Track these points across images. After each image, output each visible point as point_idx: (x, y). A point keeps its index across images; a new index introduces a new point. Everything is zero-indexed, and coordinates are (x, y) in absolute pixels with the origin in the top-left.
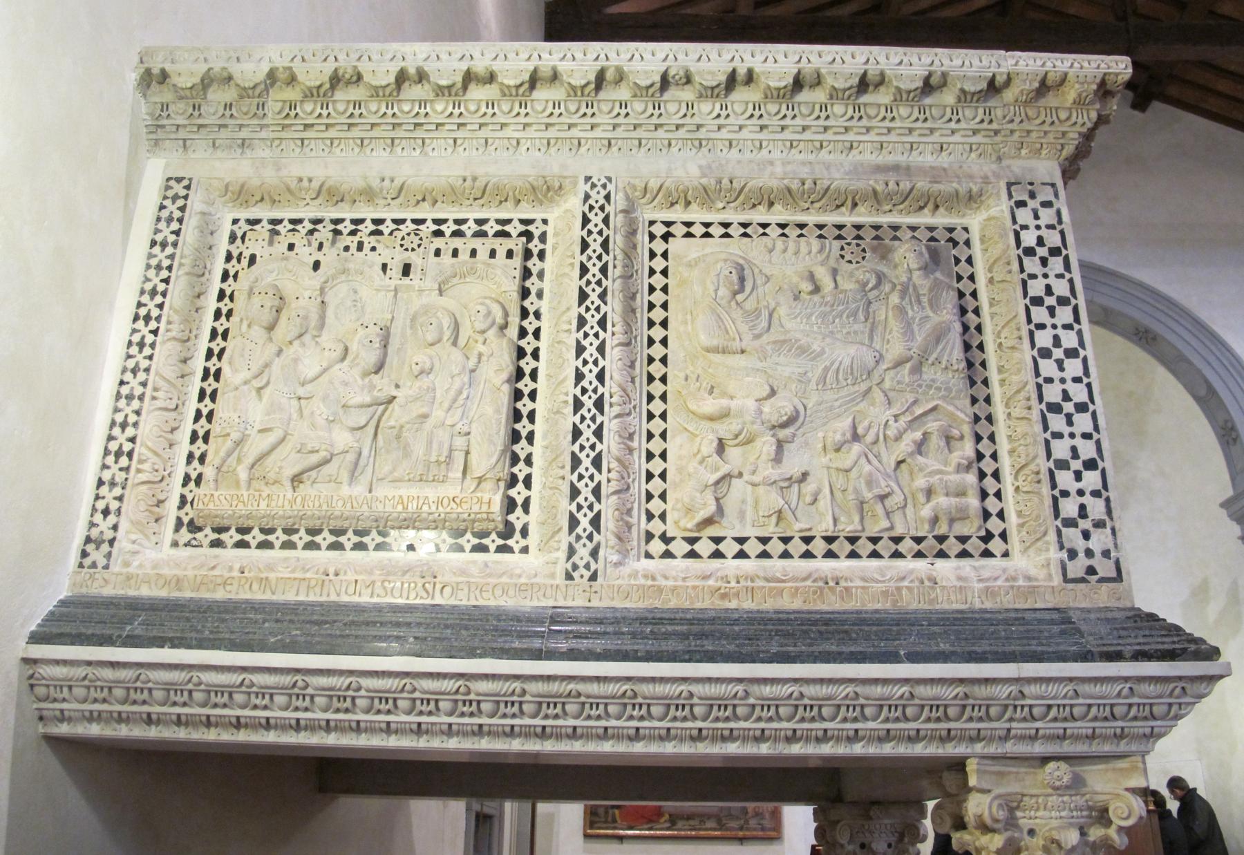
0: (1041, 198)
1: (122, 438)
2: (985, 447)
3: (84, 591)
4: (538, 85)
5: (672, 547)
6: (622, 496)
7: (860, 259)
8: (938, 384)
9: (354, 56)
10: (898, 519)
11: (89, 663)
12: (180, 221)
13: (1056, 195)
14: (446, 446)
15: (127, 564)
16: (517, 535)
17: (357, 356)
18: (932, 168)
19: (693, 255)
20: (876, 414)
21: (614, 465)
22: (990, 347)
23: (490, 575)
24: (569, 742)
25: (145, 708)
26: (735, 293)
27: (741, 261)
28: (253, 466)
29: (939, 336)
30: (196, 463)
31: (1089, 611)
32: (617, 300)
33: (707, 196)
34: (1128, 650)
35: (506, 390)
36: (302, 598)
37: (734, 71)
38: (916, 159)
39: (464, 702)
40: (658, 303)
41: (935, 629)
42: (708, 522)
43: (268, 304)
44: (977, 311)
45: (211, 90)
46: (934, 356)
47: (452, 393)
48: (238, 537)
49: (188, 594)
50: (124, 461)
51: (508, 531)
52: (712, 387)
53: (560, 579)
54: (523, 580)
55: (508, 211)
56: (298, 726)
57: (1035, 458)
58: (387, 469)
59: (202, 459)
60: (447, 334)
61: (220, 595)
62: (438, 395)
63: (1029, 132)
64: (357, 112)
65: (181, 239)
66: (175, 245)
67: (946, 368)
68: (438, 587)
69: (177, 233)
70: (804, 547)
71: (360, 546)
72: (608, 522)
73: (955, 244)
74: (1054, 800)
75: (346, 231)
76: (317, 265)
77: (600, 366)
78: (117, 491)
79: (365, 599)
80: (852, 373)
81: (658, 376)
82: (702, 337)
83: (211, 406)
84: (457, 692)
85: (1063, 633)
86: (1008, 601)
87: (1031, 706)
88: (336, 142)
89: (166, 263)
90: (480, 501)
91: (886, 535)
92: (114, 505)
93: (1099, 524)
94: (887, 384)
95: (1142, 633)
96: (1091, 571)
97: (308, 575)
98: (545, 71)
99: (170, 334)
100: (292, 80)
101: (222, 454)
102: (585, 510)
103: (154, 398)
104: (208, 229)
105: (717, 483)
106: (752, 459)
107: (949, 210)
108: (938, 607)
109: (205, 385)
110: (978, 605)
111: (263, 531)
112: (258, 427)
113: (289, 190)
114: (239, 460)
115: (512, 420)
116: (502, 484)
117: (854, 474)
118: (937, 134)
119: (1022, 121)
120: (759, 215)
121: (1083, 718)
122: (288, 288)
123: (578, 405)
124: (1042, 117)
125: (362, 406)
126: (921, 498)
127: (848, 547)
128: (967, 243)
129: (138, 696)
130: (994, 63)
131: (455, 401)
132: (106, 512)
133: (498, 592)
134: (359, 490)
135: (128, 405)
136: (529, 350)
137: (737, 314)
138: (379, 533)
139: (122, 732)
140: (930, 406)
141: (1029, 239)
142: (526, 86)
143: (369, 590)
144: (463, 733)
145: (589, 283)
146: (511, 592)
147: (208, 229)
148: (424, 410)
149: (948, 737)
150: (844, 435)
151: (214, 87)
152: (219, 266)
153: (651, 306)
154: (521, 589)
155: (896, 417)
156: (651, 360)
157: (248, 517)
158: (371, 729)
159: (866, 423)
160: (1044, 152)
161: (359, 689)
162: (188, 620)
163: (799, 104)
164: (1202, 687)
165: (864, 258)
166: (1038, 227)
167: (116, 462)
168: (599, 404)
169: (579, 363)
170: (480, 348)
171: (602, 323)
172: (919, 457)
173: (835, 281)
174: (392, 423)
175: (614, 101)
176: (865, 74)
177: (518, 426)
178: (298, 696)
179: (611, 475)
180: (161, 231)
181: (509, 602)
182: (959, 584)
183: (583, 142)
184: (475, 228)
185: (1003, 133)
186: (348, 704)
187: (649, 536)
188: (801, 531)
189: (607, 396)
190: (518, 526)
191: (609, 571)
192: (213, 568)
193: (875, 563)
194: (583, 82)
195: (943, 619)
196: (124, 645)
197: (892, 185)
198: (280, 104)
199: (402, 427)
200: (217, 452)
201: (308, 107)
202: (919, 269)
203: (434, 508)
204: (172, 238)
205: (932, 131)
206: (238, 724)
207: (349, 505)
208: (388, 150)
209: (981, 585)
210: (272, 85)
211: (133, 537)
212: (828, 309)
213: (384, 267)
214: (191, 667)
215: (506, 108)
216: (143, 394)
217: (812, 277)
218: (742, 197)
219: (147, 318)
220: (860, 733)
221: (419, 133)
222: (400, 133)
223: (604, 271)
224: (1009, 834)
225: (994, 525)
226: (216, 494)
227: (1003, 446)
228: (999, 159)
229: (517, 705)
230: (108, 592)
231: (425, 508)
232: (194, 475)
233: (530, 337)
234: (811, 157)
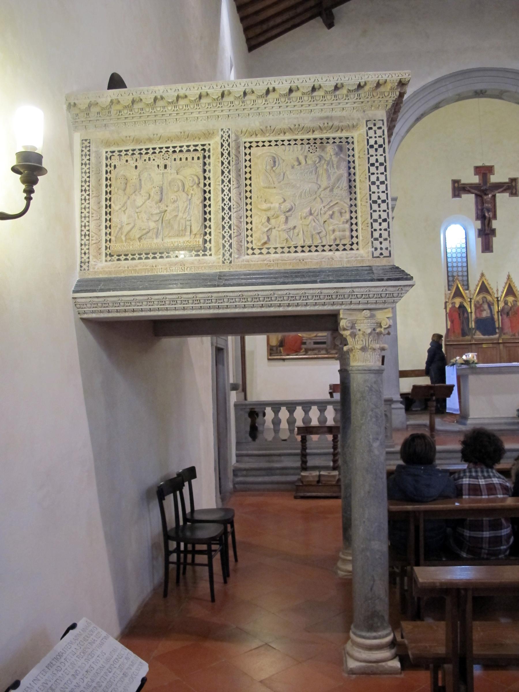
0: (377, 126)
1: (85, 231)
2: (354, 215)
3: (83, 277)
4: (202, 98)
5: (255, 251)
6: (238, 237)
7: (315, 152)
8: (338, 195)
9: (139, 93)
10: (324, 240)
11: (91, 297)
12: (89, 155)
13: (383, 124)
14: (184, 224)
15: (94, 268)
16: (208, 251)
17: (153, 197)
18: (340, 117)
19: (259, 153)
20: (318, 206)
21: (235, 228)
22: (357, 180)
23: (201, 264)
24: (226, 310)
25: (108, 308)
26: (272, 168)
27: (274, 156)
28: (126, 235)
29: (338, 179)
30: (108, 235)
31: (379, 266)
32: (234, 173)
33: (263, 132)
34: (385, 278)
35: (201, 206)
36: (147, 274)
37: (268, 88)
38: (334, 114)
39: (196, 300)
40: (248, 172)
41: (330, 273)
42: (265, 243)
43: (123, 182)
44: (354, 168)
45: (91, 108)
46: (337, 185)
47: (184, 207)
48: (125, 257)
49: (114, 276)
50: (87, 237)
51: (205, 250)
52: (266, 200)
53: (221, 264)
54: (210, 264)
55: (197, 141)
56: (150, 310)
57: (367, 219)
58: (167, 233)
59: (110, 234)
60: (181, 188)
61: (123, 275)
62: (180, 209)
63: (374, 101)
64: (142, 112)
65: (91, 161)
66: (89, 164)
67: (341, 189)
68: (186, 268)
69: (89, 160)
70: (295, 250)
71: (161, 257)
72: (234, 245)
73: (348, 143)
74: (366, 321)
75: (144, 153)
76: (136, 167)
77: (229, 196)
78: (87, 247)
79: (165, 273)
80: (310, 193)
81: (249, 197)
82: (262, 184)
83: (110, 217)
84: (193, 297)
85: (369, 273)
86: (355, 264)
87: (357, 295)
88: (136, 123)
89: (88, 171)
90: (196, 241)
91: (320, 245)
92: (87, 251)
93: (385, 239)
94: (322, 196)
95: (392, 273)
96: (381, 254)
97: (148, 267)
98: (204, 94)
99: (93, 195)
100: (119, 102)
101: (116, 232)
102: (227, 242)
103: (92, 217)
104: (98, 157)
105: (267, 231)
106: (278, 223)
107: (347, 131)
108: (333, 267)
109: (107, 210)
110: (345, 265)
111: (132, 255)
112: (126, 223)
113: (123, 140)
114: (122, 234)
115: (204, 214)
116: (202, 235)
117: (310, 226)
118: (341, 104)
119: (371, 98)
120: (281, 137)
121: (373, 297)
122: (128, 175)
123: (223, 209)
124: (379, 96)
125: (157, 214)
126: (331, 233)
127: (308, 249)
128: (353, 143)
129: (105, 305)
130: (360, 78)
131: (185, 210)
132: (85, 253)
133: (203, 268)
134: (159, 240)
135: (85, 220)
136: (207, 191)
137: (273, 174)
138: (167, 253)
139: (102, 315)
140: (335, 202)
141: (372, 142)
142: (198, 99)
143: (166, 271)
144: (196, 309)
145: (224, 168)
146: (207, 268)
147: (98, 157)
148: (176, 214)
149: (333, 304)
150: (306, 214)
151: (92, 106)
152: (104, 169)
153: (246, 173)
154: (210, 267)
155: (324, 207)
156: (246, 191)
157: (127, 251)
158: (171, 310)
159: (314, 209)
160: (380, 108)
161: (166, 299)
162: (115, 283)
163: (292, 98)
164: (407, 288)
165: (316, 151)
166: (376, 137)
167: (85, 238)
168: (230, 209)
169: (223, 196)
170: (192, 192)
171: (229, 181)
172: (331, 219)
173: (306, 161)
174: (167, 218)
175: (228, 102)
176: (314, 85)
177: (206, 216)
178: (149, 302)
179: (234, 231)
180: (84, 160)
181: (206, 271)
182: (339, 259)
183: (219, 116)
184: (186, 148)
185: (365, 102)
186: (164, 303)
187: (248, 248)
188: (293, 245)
189: (232, 206)
190: (208, 248)
191: (235, 260)
192: (119, 267)
193: (316, 253)
194: (217, 97)
195: (333, 270)
196: (99, 292)
197: (326, 124)
198: (116, 111)
199: (170, 220)
200: (114, 232)
201: (126, 111)
202: (334, 155)
203: (182, 244)
204: (88, 162)
205: (339, 103)
206: (134, 311)
207: (157, 246)
208: (154, 124)
209: (347, 259)
210: (112, 104)
211: (94, 260)
212: (303, 171)
213: (158, 166)
214: (119, 296)
215: (192, 107)
216: (89, 216)
217: (298, 160)
218: (274, 132)
219: (85, 190)
220: (308, 304)
221: (164, 118)
222: (157, 118)
223: (229, 163)
224: (352, 330)
225: (355, 240)
226: (116, 245)
227: (359, 214)
228: (364, 111)
229: (210, 300)
230: (90, 277)
231: (180, 244)
232: (108, 239)
233: (207, 186)
234: (298, 116)
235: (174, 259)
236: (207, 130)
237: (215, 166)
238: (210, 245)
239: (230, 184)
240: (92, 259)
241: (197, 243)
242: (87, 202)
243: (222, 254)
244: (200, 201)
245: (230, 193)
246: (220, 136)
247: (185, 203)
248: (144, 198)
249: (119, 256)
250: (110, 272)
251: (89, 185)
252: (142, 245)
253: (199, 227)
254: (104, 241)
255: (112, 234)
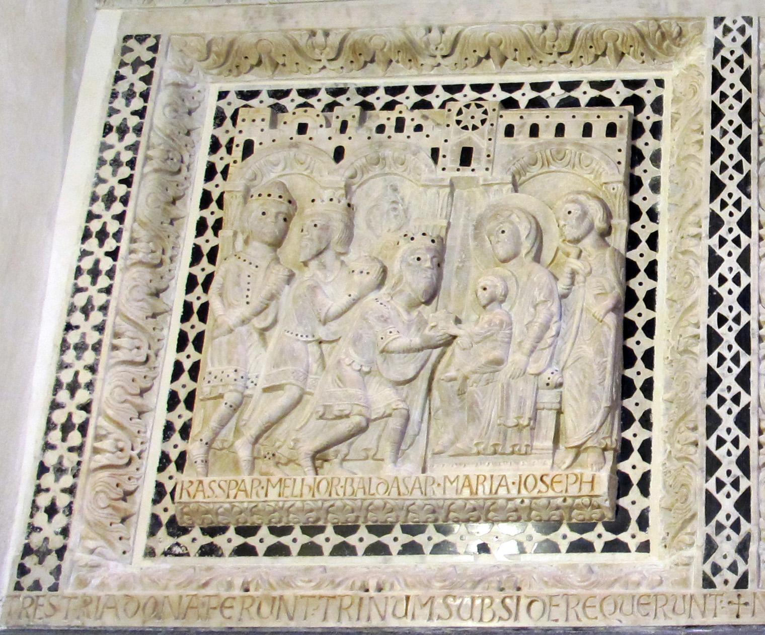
12: (145, 96)
14: (529, 403)
15: (83, 583)
16: (633, 527)
17: (400, 280)
23: (596, 584)
28: (257, 439)
30: (176, 438)
36: (331, 623)
43: (272, 211)
47: (536, 328)
48: (239, 540)
50: (75, 438)
51: (619, 522)
53: (695, 587)
54: (643, 590)
55: (608, 70)
58: (446, 438)
59: (185, 432)
60: (526, 245)
62: (516, 330)
65: (146, 121)
66: (138, 130)
68: (524, 602)
69: (141, 113)
71: (412, 549)
75: (379, 105)
76: (339, 154)
78: (67, 481)
89: (126, 156)
90: (579, 479)
92: (63, 500)
97: (340, 591)
99: (134, 257)
101: (213, 423)
102: (728, 488)
103: (115, 348)
109: (186, 327)
112: (262, 383)
113: (297, 48)
114: (238, 432)
115: (621, 364)
116: (610, 455)
122: (300, 187)
123: (714, 340)
125: (408, 351)
131: (539, 339)
132: (51, 511)
133: (608, 607)
134: (408, 469)
135: (78, 358)
136: (642, 264)
138: (439, 529)
143: (426, 611)
145: (724, 167)
146: (627, 608)
148: (497, 353)
152: (201, 158)
154: (641, 602)
167: (64, 439)
169: (714, 281)
174: (452, 373)
177: (630, 373)
180: (118, 111)
184: (561, 94)
189: (754, 326)
190: (634, 514)
199: (466, 378)
200: (205, 421)
203: (514, 492)
204: (133, 121)
207: (394, 491)
211: (91, 544)
213: (435, 153)
219: (102, 235)
226: (206, 480)
231: (502, 492)
233: (643, 247)
235: (469, 559)
236: (656, 20)
237: (683, 159)
238: (643, 503)
239: (748, 233)
240: (83, 538)
241: (586, 490)
242: (103, 282)
243: (700, 541)
244: (609, 302)
245: (748, 272)
246: (711, 45)
247: (540, 308)
248: (356, 277)
249: (212, 531)
250: (157, 606)
251: (124, 213)
252: (324, 485)
253: (597, 421)
254: (153, 460)
255: (194, 431)
